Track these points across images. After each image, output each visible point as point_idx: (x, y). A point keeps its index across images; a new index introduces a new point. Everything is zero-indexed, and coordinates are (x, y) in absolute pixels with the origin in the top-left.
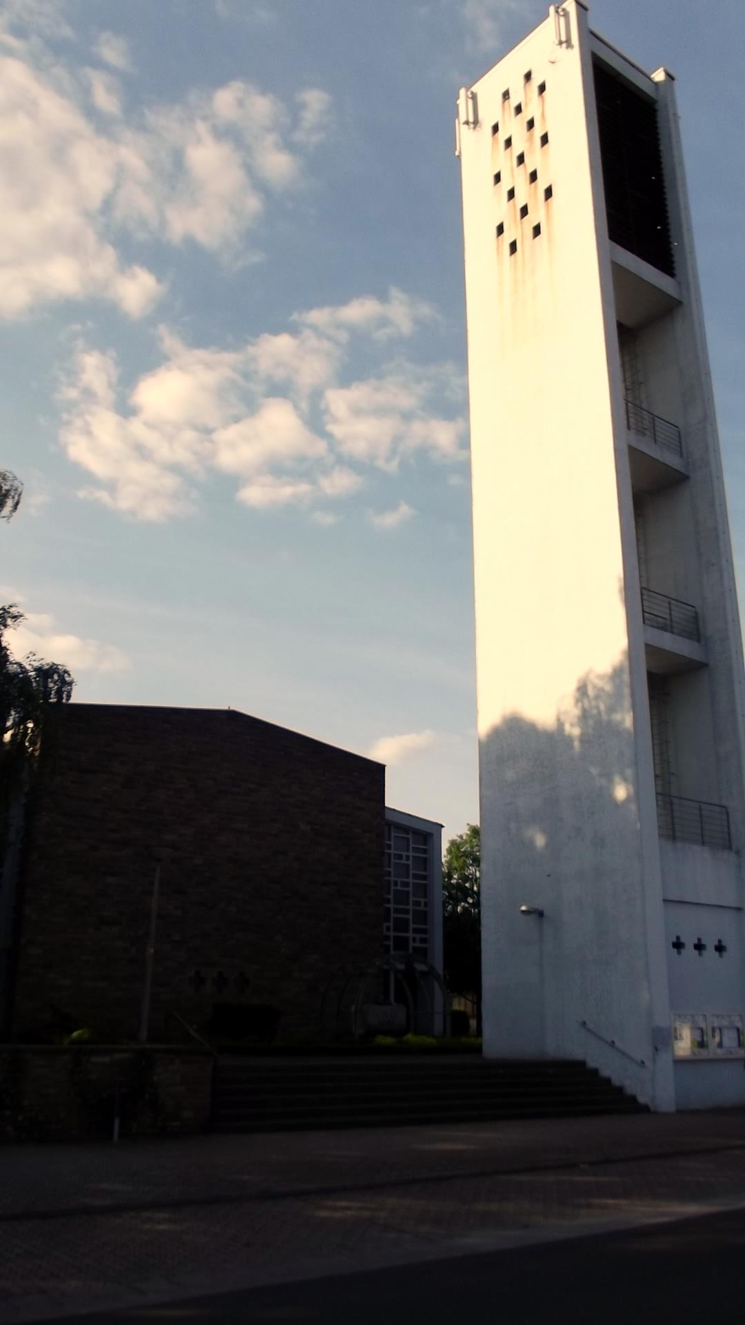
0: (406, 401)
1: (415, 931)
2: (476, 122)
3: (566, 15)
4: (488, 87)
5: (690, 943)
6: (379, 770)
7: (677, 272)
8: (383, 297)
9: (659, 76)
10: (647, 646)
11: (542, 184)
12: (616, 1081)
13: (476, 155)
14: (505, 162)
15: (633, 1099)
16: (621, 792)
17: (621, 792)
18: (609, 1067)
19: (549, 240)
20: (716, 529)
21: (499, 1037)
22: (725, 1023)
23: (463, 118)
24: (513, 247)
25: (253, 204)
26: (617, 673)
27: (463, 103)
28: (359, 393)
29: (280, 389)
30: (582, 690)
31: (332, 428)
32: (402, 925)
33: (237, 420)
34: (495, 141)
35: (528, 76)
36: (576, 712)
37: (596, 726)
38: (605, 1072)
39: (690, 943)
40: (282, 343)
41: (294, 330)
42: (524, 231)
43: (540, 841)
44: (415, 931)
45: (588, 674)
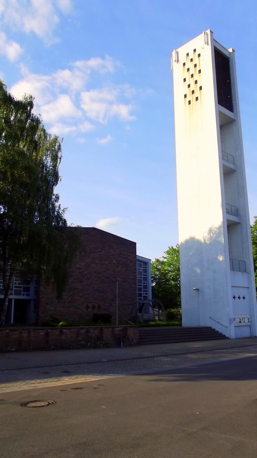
0: (110, 97)
1: (144, 291)
2: (178, 61)
3: (207, 34)
4: (183, 50)
5: (237, 297)
6: (135, 243)
7: (234, 111)
8: (103, 58)
9: (231, 50)
10: (227, 220)
11: (199, 85)
12: (220, 332)
13: (178, 72)
14: (187, 76)
15: (225, 336)
16: (221, 258)
17: (221, 258)
18: (218, 328)
19: (201, 102)
20: (243, 186)
21: (187, 321)
22: (237, 316)
23: (174, 59)
24: (190, 102)
25: (56, 19)
26: (220, 228)
27: (174, 53)
28: (93, 94)
29: (65, 91)
30: (210, 231)
31: (83, 106)
32: (140, 290)
33: (49, 102)
34: (184, 68)
35: (195, 50)
36: (208, 237)
37: (214, 242)
38: (217, 330)
39: (237, 297)
40: (66, 73)
41: (71, 69)
42: (192, 98)
43: (199, 271)
44: (144, 291)
45: (212, 227)
